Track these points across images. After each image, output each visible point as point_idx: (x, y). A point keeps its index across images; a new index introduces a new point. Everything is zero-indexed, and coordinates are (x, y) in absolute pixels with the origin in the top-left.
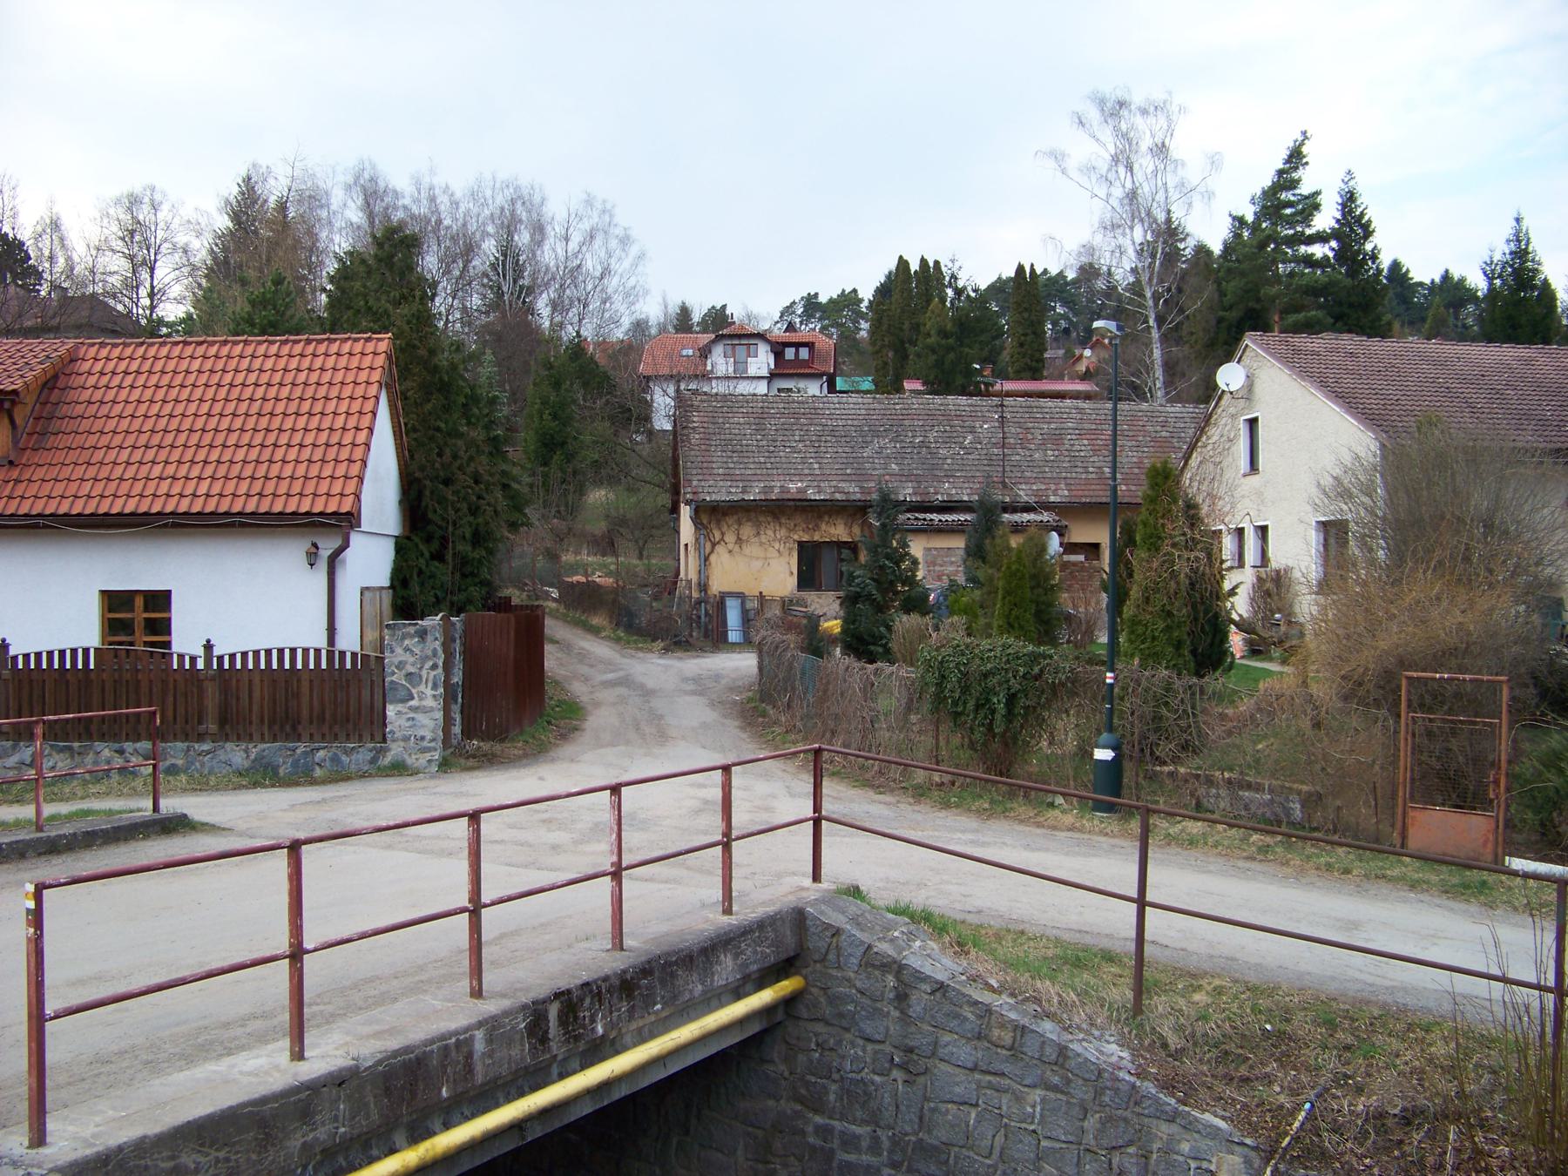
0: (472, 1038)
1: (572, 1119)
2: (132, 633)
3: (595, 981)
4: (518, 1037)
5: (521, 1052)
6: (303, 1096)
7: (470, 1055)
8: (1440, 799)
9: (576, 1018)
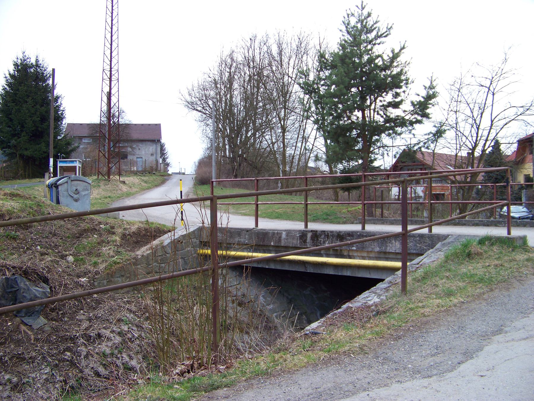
0: (282, 233)
1: (325, 273)
2: (521, 201)
3: (327, 231)
4: (296, 238)
5: (297, 242)
6: (239, 230)
7: (280, 237)
8: (205, 160)
9: (317, 240)
